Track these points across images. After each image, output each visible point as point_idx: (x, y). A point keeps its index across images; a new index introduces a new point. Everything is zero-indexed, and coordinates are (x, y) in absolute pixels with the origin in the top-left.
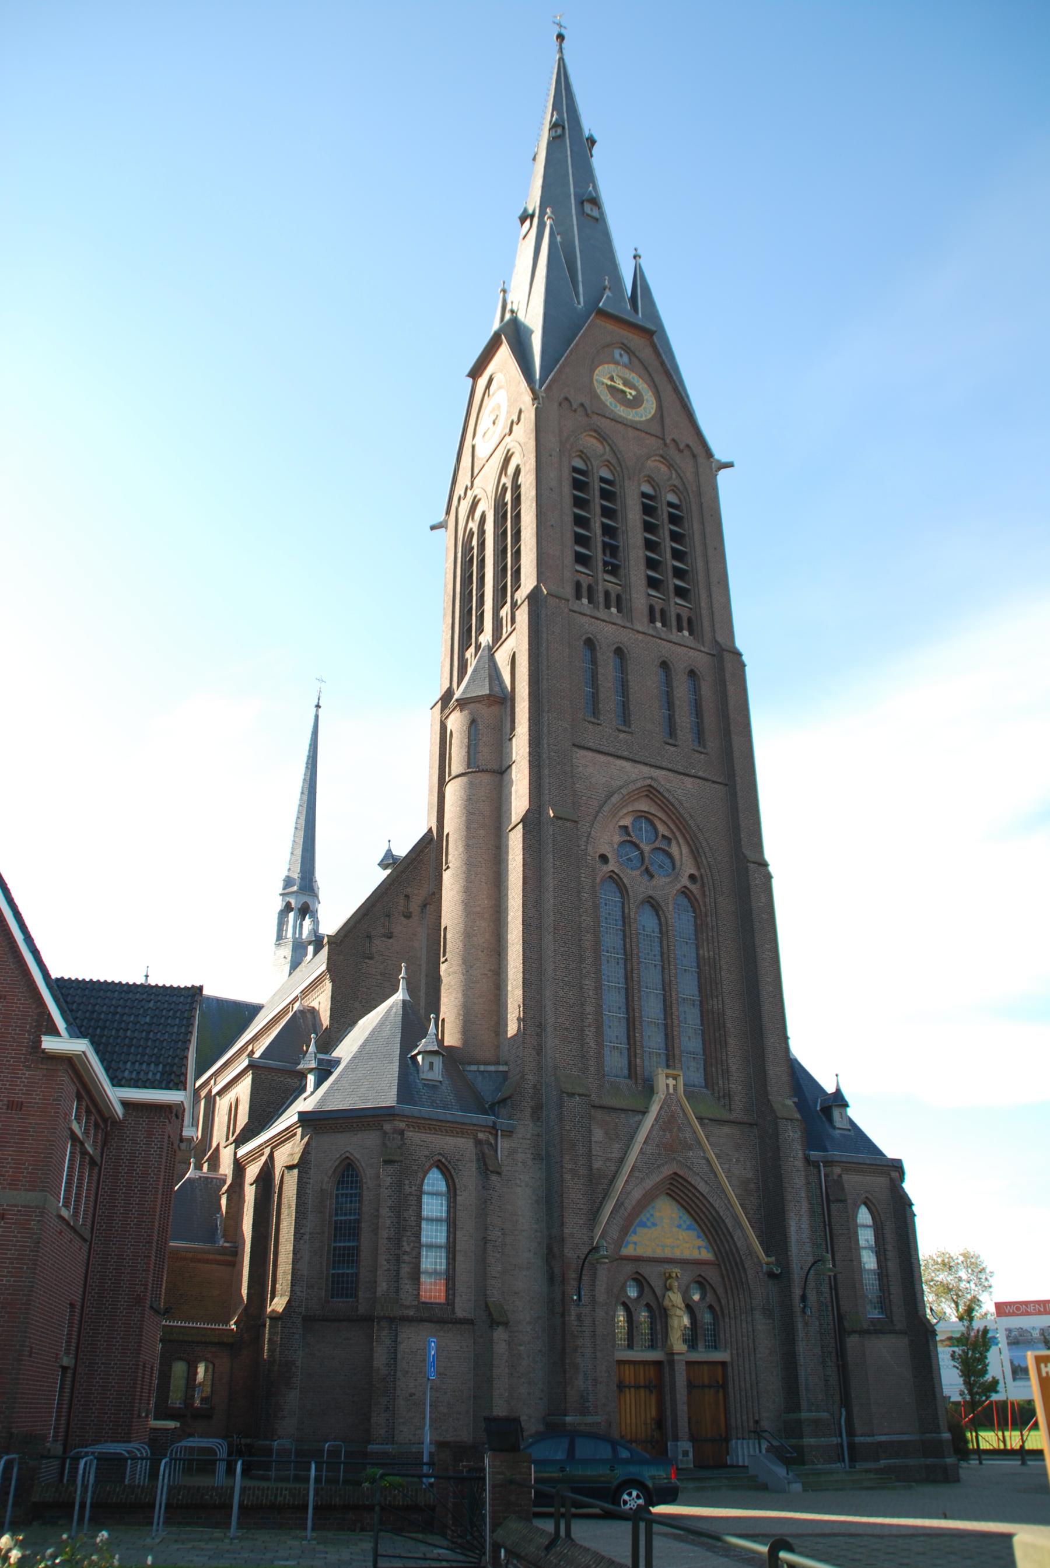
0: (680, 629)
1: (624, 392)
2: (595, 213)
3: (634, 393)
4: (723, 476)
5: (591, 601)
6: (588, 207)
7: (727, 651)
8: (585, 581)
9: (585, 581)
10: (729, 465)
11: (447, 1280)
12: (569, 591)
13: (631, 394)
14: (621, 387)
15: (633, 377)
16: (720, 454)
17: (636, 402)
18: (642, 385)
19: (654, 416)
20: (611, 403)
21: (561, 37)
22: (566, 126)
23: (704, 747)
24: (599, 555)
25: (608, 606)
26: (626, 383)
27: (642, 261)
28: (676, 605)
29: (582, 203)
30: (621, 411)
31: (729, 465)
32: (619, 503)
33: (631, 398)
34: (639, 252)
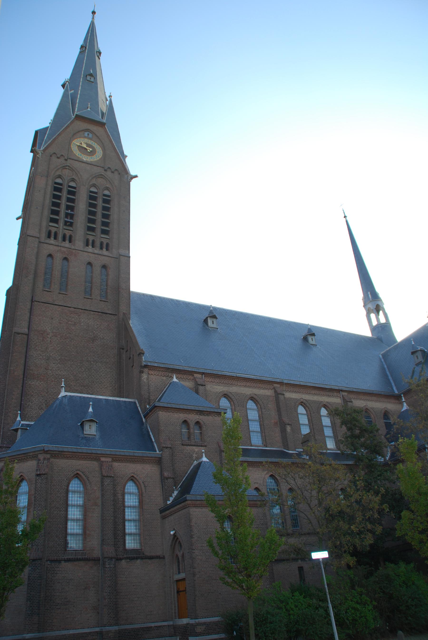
0: (101, 248)
1: (87, 149)
2: (92, 80)
3: (91, 149)
4: (133, 183)
5: (93, 246)
6: (88, 78)
7: (122, 255)
8: (53, 230)
9: (53, 230)
10: (136, 176)
11: (260, 422)
12: (44, 235)
13: (89, 150)
14: (85, 147)
15: (90, 142)
16: (132, 172)
17: (93, 153)
18: (96, 146)
19: (101, 158)
20: (78, 154)
21: (94, 13)
22: (87, 48)
23: (91, 296)
24: (98, 226)
25: (101, 248)
26: (88, 145)
27: (112, 98)
28: (99, 237)
29: (86, 76)
30: (85, 158)
31: (136, 176)
32: (77, 196)
33: (89, 151)
34: (112, 94)
